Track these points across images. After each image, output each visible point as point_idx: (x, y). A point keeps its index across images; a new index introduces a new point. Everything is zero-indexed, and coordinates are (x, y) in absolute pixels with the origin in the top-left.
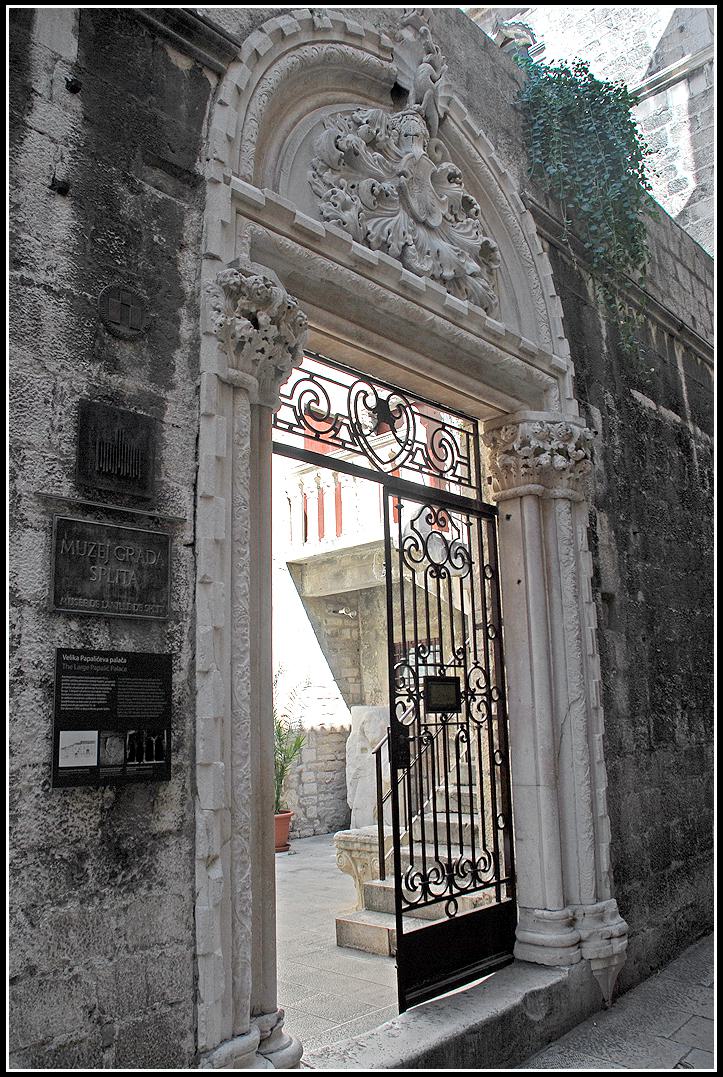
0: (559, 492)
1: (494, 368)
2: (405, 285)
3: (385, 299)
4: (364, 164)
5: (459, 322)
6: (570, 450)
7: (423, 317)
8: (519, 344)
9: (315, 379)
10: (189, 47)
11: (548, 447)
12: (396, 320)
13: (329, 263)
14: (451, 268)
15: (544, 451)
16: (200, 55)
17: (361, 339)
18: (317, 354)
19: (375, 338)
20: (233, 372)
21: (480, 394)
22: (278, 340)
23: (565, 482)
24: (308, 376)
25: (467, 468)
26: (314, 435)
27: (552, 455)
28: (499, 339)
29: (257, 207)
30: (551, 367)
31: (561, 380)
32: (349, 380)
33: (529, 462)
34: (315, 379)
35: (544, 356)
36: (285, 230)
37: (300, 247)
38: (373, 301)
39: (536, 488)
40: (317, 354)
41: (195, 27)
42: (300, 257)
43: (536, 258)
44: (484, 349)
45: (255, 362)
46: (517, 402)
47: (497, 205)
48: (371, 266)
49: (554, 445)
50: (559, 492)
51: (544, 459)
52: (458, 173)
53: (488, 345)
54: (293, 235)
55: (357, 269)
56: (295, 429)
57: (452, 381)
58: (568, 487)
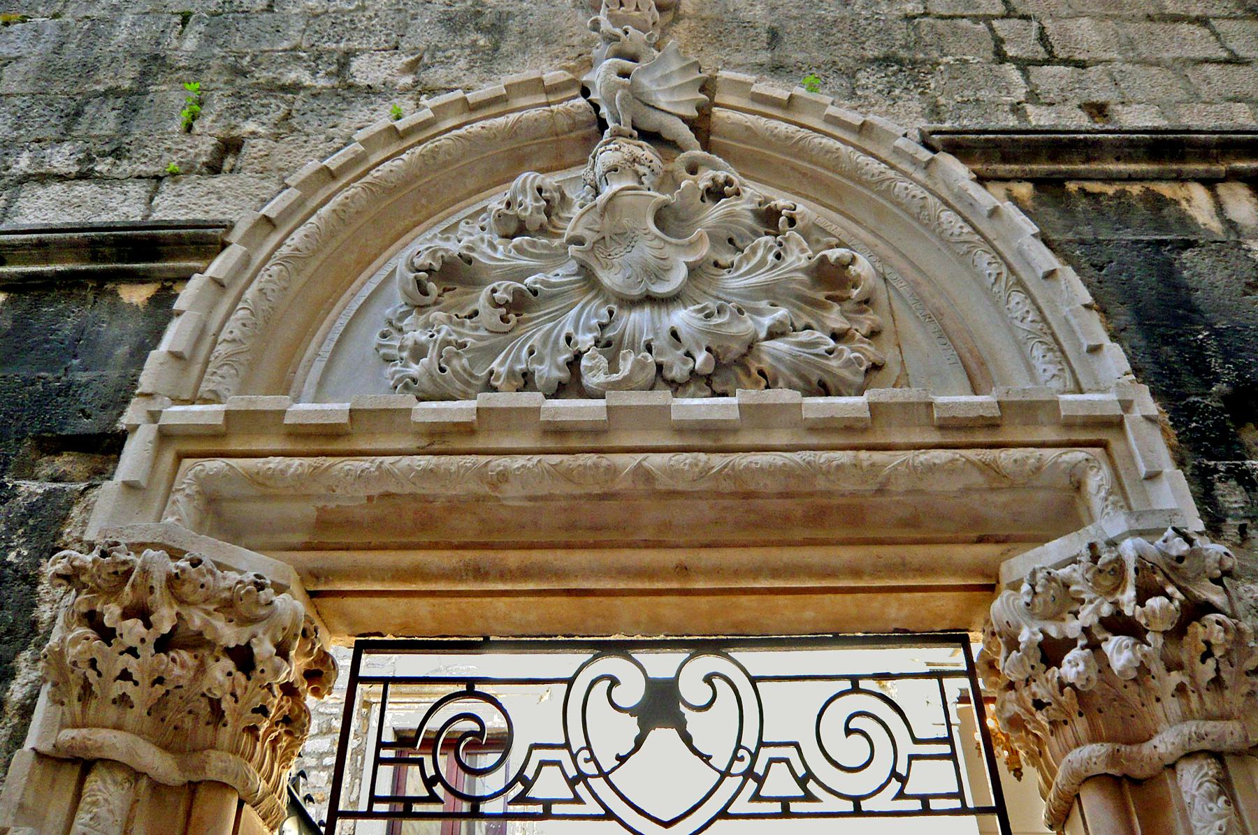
0: (1165, 743)
1: (884, 500)
2: (558, 431)
3: (504, 476)
4: (487, 267)
5: (730, 441)
6: (1128, 612)
7: (613, 471)
8: (930, 416)
9: (478, 688)
10: (145, 270)
11: (1072, 628)
12: (563, 504)
13: (901, 456)
14: (700, 349)
15: (1070, 644)
16: (160, 270)
17: (479, 573)
18: (836, 635)
19: (513, 558)
20: (67, 734)
21: (856, 573)
22: (164, 644)
23: (1173, 705)
24: (847, 685)
25: (951, 763)
26: (849, 806)
27: (1094, 646)
28: (864, 430)
29: (215, 434)
30: (943, 427)
31: (1116, 446)
32: (563, 663)
33: (1041, 690)
34: (478, 688)
35: (1028, 411)
36: (276, 445)
37: (565, 457)
38: (485, 490)
39: (1092, 754)
40: (486, 638)
41: (154, 240)
42: (298, 476)
43: (984, 226)
44: (812, 471)
45: (124, 700)
46: (987, 551)
47: (866, 184)
48: (466, 429)
49: (1087, 616)
50: (1165, 743)
51: (1073, 666)
52: (721, 180)
53: (824, 456)
54: (949, 439)
55: (436, 447)
56: (795, 807)
57: (876, 572)
58: (1186, 716)
